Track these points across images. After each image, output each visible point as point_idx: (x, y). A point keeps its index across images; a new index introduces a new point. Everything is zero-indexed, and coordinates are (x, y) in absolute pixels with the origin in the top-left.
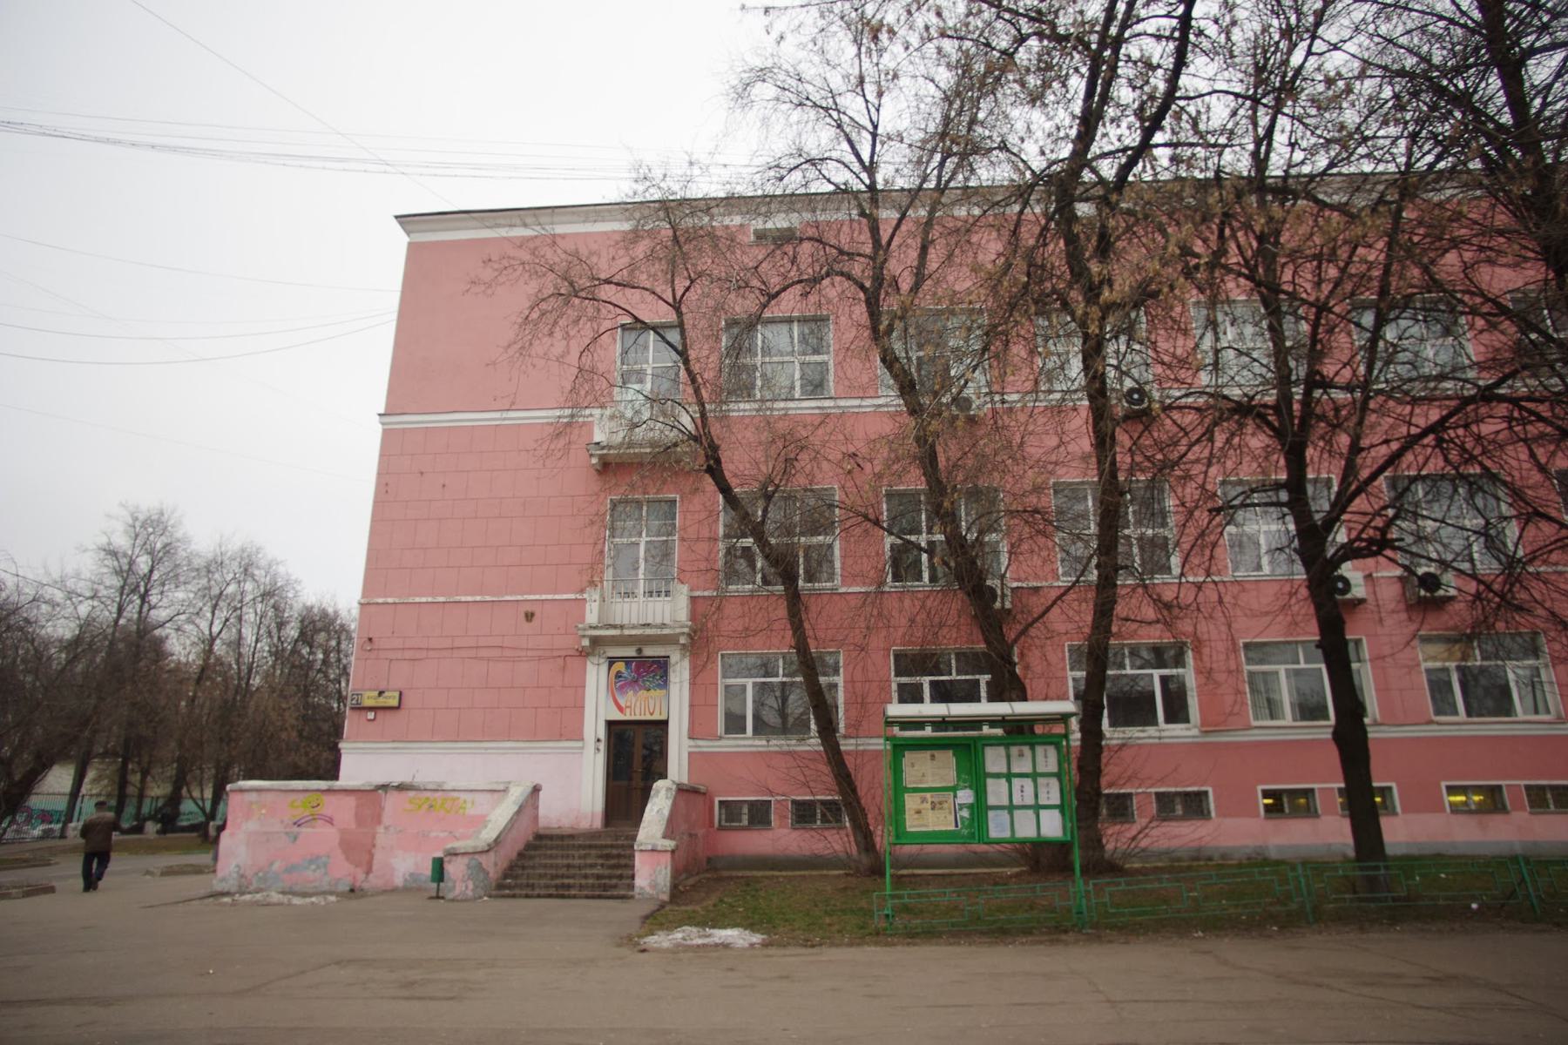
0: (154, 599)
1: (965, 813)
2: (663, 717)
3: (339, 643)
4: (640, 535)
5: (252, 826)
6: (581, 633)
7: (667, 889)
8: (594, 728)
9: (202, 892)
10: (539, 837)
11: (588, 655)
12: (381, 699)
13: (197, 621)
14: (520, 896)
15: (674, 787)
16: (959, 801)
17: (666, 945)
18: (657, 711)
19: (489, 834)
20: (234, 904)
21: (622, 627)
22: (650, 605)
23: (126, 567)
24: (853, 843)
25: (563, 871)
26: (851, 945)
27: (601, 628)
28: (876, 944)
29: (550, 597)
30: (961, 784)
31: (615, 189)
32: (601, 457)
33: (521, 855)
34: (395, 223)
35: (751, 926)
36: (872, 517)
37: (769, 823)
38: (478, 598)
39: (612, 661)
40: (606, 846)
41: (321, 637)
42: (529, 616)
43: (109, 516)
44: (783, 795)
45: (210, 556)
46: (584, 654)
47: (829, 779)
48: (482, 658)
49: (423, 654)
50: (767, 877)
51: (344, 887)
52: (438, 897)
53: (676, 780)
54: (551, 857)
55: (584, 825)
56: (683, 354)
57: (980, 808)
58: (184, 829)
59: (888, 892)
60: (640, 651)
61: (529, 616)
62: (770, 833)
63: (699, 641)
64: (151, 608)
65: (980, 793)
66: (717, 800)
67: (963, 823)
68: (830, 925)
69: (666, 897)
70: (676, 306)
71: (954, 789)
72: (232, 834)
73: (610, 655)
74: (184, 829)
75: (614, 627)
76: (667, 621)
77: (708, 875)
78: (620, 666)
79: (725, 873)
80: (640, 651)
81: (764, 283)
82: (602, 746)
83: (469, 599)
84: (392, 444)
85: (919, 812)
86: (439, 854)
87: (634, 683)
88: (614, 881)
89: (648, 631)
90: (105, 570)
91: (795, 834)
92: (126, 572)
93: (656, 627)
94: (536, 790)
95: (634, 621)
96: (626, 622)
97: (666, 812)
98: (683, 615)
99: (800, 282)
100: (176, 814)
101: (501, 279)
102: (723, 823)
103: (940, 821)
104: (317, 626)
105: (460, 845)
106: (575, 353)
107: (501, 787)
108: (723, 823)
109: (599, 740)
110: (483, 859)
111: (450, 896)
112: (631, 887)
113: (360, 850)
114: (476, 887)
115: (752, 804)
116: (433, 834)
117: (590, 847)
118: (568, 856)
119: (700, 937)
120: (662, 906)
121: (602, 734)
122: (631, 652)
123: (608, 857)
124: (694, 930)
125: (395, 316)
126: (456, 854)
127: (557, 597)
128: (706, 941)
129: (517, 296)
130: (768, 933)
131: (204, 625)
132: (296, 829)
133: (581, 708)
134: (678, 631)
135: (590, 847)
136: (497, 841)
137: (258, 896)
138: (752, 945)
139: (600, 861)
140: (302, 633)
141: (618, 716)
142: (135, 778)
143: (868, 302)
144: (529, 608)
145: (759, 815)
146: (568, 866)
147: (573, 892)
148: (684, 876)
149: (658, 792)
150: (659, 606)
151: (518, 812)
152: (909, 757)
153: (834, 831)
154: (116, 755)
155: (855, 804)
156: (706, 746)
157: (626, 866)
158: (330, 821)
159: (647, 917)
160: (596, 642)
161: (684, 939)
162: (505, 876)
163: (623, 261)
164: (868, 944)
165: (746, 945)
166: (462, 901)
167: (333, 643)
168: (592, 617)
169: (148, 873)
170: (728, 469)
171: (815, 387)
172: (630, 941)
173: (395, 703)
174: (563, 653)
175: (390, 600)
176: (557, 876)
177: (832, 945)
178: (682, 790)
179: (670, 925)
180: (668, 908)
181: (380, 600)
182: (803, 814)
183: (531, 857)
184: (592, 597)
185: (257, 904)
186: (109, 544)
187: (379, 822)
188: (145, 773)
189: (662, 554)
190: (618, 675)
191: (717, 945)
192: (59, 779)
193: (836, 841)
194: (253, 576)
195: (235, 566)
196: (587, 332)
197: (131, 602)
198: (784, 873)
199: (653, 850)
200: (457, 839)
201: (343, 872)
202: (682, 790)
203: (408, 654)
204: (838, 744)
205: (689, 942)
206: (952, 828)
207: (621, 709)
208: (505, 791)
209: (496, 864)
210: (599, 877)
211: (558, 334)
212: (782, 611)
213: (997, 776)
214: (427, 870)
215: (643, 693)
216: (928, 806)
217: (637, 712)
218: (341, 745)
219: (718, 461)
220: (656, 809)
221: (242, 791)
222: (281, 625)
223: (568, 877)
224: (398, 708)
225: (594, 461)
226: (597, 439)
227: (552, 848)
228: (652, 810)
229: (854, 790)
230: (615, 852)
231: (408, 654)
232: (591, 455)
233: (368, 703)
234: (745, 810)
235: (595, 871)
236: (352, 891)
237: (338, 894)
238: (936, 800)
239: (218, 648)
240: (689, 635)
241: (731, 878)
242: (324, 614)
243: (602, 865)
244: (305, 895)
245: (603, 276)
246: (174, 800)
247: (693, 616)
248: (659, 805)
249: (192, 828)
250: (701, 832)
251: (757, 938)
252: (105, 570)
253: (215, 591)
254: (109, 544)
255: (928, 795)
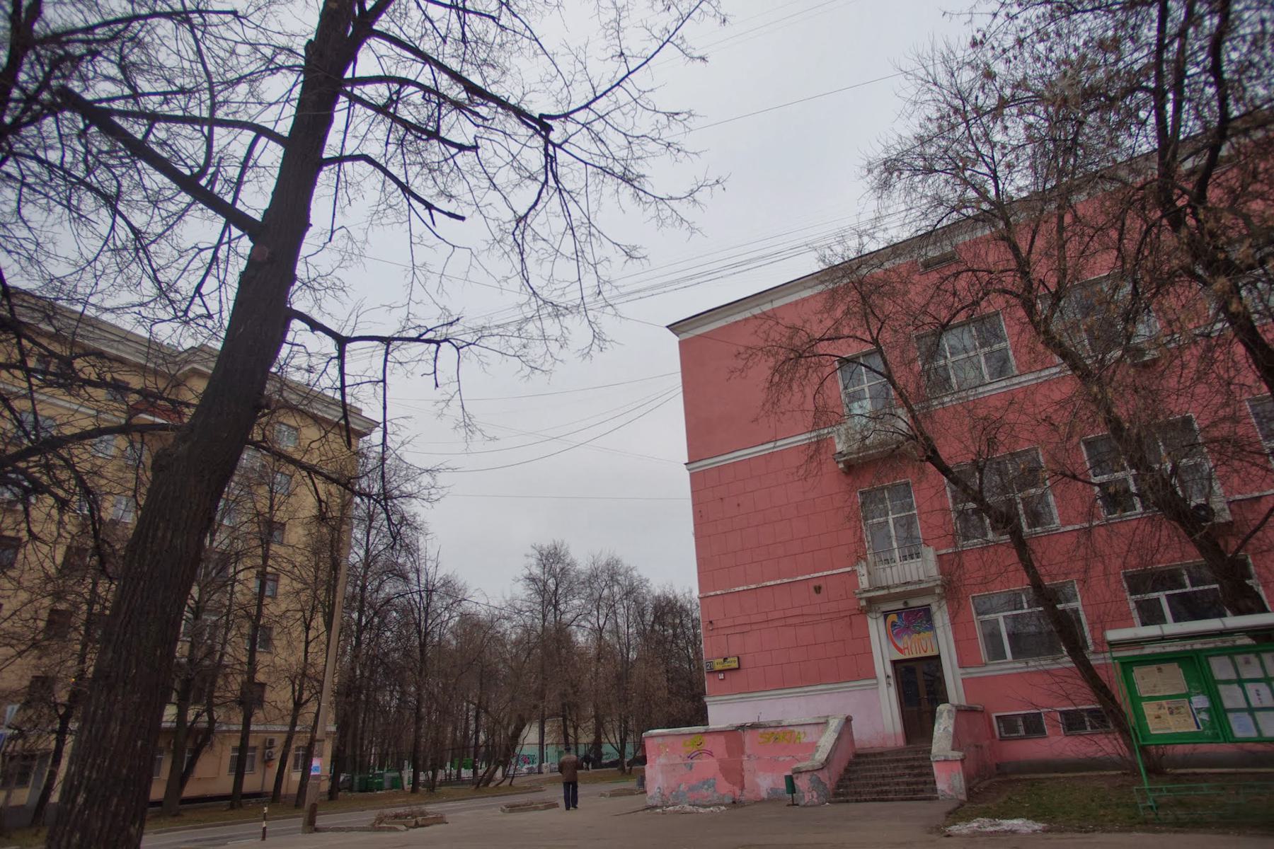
0: (562, 607)
1: (1204, 716)
2: (935, 653)
3: (681, 621)
4: (887, 515)
5: (662, 760)
6: (858, 596)
7: (963, 791)
8: (882, 667)
9: (641, 806)
10: (857, 756)
11: (867, 612)
12: (726, 664)
13: (589, 618)
14: (852, 801)
15: (954, 709)
16: (1194, 706)
17: (965, 831)
18: (929, 648)
19: (821, 756)
20: (664, 813)
21: (888, 587)
22: (906, 567)
23: (542, 588)
24: (1123, 746)
25: (880, 780)
26: (1120, 831)
27: (873, 591)
28: (1144, 831)
29: (829, 573)
30: (1192, 690)
31: (809, 265)
32: (844, 462)
33: (846, 770)
34: (667, 330)
35: (1035, 818)
36: (1069, 473)
37: (1044, 732)
38: (779, 582)
39: (886, 615)
40: (909, 760)
41: (669, 619)
42: (818, 589)
43: (527, 556)
44: (1052, 707)
45: (589, 572)
46: (864, 612)
47: (1086, 690)
48: (790, 625)
49: (748, 628)
50: (1047, 778)
51: (728, 800)
52: (794, 805)
53: (956, 703)
54: (869, 770)
55: (891, 744)
56: (889, 377)
57: (1218, 712)
58: (607, 765)
59: (1147, 786)
60: (906, 603)
61: (818, 589)
62: (1041, 741)
63: (951, 589)
64: (562, 613)
65: (1215, 698)
66: (994, 716)
67: (1204, 725)
68: (1104, 816)
69: (963, 797)
70: (875, 341)
71: (1187, 696)
72: (651, 766)
73: (884, 609)
74: (607, 765)
75: (883, 588)
76: (922, 578)
77: (997, 779)
78: (893, 617)
79: (1015, 777)
80: (906, 603)
81: (935, 318)
82: (892, 681)
83: (772, 583)
84: (698, 481)
85: (1158, 717)
86: (789, 773)
87: (907, 629)
88: (921, 787)
89: (910, 588)
90: (530, 592)
91: (1066, 740)
92: (543, 591)
93: (915, 583)
94: (848, 720)
95: (897, 581)
96: (890, 583)
97: (951, 729)
98: (934, 571)
99: (963, 308)
100: (599, 755)
101: (750, 364)
102: (1003, 734)
103: (1180, 724)
104: (667, 609)
105: (803, 765)
106: (810, 398)
107: (822, 721)
108: (1003, 734)
109: (888, 677)
110: (820, 774)
111: (802, 803)
112: (935, 790)
113: (733, 773)
114: (819, 796)
115: (1025, 717)
116: (781, 759)
117: (898, 761)
118: (881, 769)
119: (992, 826)
120: (962, 805)
121: (890, 671)
122: (899, 605)
123: (912, 767)
124: (986, 820)
125: (681, 389)
126: (801, 772)
127: (835, 572)
128: (997, 828)
129: (762, 369)
130: (1049, 822)
131: (594, 620)
132: (690, 761)
133: (870, 653)
134: (932, 584)
135: (898, 761)
136: (828, 760)
137: (677, 808)
138: (1035, 831)
139: (907, 771)
140: (656, 617)
141: (899, 656)
142: (571, 731)
143: (1024, 305)
144: (816, 583)
145: (1034, 726)
146: (884, 777)
147: (891, 797)
148: (977, 781)
149: (941, 713)
150: (913, 566)
151: (838, 739)
152: (1137, 672)
153: (1103, 736)
154: (558, 715)
155: (1116, 711)
156: (975, 672)
157: (928, 774)
158: (711, 754)
159: (950, 813)
160: (870, 601)
161: (979, 827)
162: (839, 787)
163: (829, 323)
164: (1136, 831)
165: (1030, 830)
166: (811, 806)
167: (678, 621)
168: (864, 582)
169: (602, 795)
170: (944, 453)
171: (1001, 370)
172: (938, 830)
173: (735, 665)
174: (848, 613)
175: (718, 592)
176: (876, 785)
177: (1104, 831)
178: (960, 711)
179: (968, 818)
180: (967, 806)
181: (712, 594)
182: (1073, 722)
183: (855, 771)
184: (862, 569)
185: (677, 812)
186: (531, 574)
187: (743, 753)
188: (576, 729)
189: (907, 524)
190: (894, 624)
191: (1006, 832)
192: (531, 735)
193: (1106, 745)
194: (617, 581)
195: (605, 576)
196: (815, 379)
197: (549, 611)
198: (1066, 775)
199: (945, 760)
200: (798, 761)
201: (725, 789)
202: (960, 711)
203: (738, 630)
204: (1088, 661)
205: (983, 830)
206: (1194, 729)
207: (900, 650)
208: (826, 723)
209: (830, 778)
210: (908, 784)
211: (795, 387)
212: (1012, 557)
213: (1228, 682)
214: (782, 785)
215: (915, 636)
216: (1166, 711)
217: (914, 650)
218: (706, 699)
219: (934, 451)
220: (942, 728)
221: (652, 737)
222: (642, 615)
223: (885, 785)
224: (739, 668)
225: (841, 466)
226: (838, 450)
227: (868, 764)
228: (939, 729)
229: (1113, 699)
230: (916, 764)
231: (738, 630)
232: (838, 462)
233: (718, 667)
234: (1020, 722)
235: (905, 780)
236: (734, 802)
237: (726, 805)
238: (1173, 706)
239: (607, 636)
240: (942, 586)
241: (1019, 780)
242: (669, 601)
243: (909, 774)
244: (705, 806)
245: (817, 336)
246: (597, 744)
247: (942, 572)
248: (944, 725)
249: (612, 764)
250: (986, 743)
251: (1038, 826)
252: (530, 592)
253: (596, 595)
254: (531, 574)
255: (1164, 702)
